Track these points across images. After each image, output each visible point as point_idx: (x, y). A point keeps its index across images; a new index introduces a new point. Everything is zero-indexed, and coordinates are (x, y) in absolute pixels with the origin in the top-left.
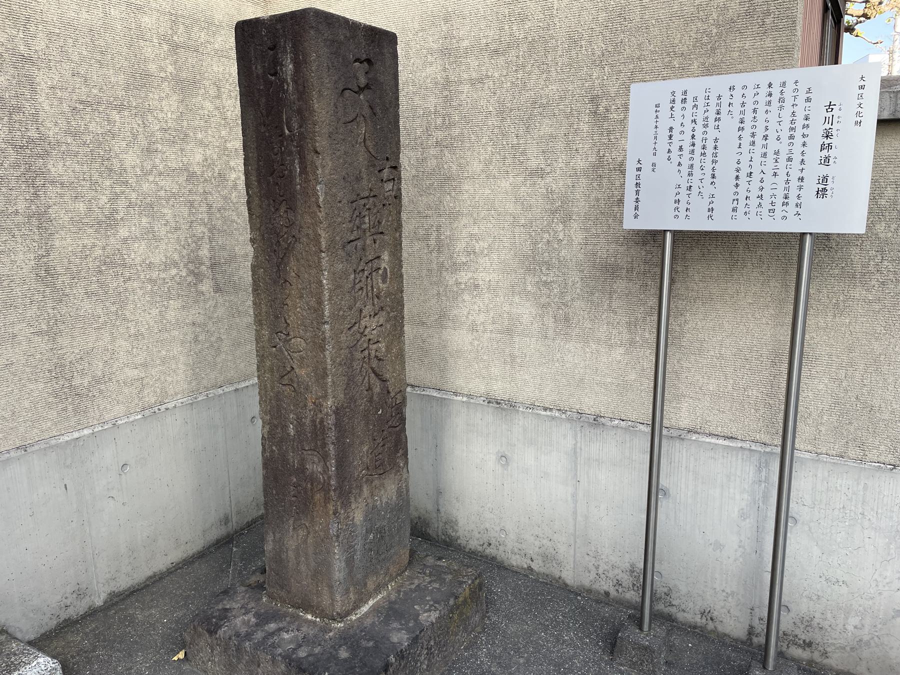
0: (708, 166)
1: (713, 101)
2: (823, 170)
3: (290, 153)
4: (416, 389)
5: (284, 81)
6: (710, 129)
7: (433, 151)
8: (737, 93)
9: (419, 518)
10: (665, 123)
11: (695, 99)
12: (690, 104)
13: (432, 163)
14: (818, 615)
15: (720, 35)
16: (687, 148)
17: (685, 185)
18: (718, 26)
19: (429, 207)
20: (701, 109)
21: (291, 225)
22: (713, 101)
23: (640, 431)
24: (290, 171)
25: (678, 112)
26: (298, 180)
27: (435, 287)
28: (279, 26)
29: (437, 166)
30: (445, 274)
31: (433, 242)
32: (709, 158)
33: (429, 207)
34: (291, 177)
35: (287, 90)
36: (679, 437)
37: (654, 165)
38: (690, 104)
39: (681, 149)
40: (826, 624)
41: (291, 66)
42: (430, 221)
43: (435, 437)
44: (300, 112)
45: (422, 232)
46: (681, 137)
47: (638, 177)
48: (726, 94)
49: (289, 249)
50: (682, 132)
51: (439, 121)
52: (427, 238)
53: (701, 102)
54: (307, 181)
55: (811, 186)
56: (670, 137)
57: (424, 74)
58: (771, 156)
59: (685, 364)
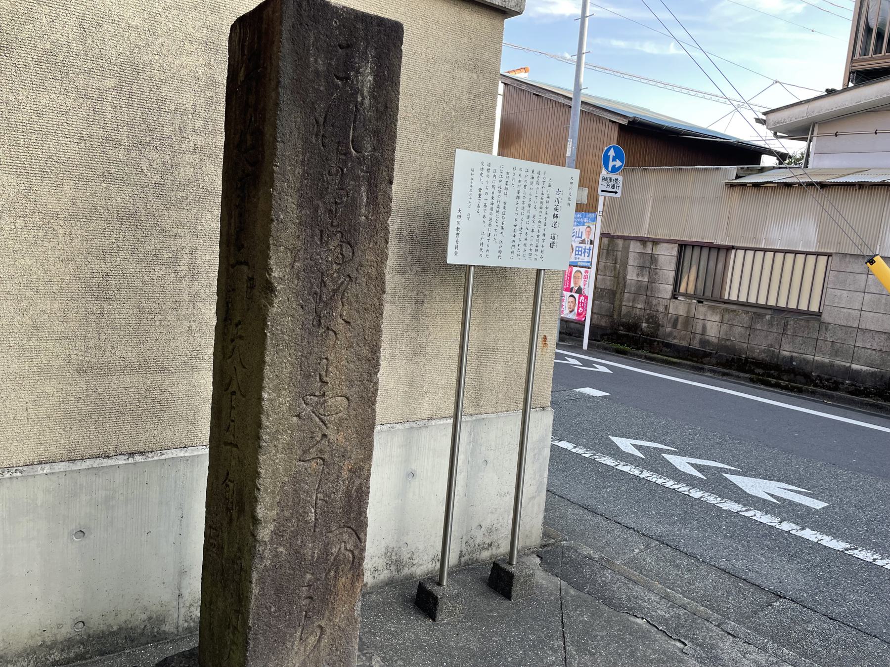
0: (500, 220)
1: (504, 175)
2: (553, 231)
3: (357, 178)
4: (150, 455)
5: (357, 91)
6: (502, 194)
7: (187, 158)
8: (517, 172)
9: (150, 618)
10: (477, 184)
11: (495, 170)
12: (491, 174)
13: (186, 172)
14: (495, 522)
15: (456, 117)
16: (489, 206)
17: (486, 233)
18: (456, 111)
19: (181, 225)
20: (498, 179)
21: (344, 261)
22: (504, 175)
23: (399, 430)
24: (354, 199)
25: (484, 179)
26: (363, 211)
27: (185, 322)
28: (360, 26)
29: (195, 175)
30: (199, 305)
31: (183, 268)
32: (501, 215)
33: (181, 225)
34: (353, 206)
35: (362, 103)
36: (425, 426)
37: (469, 215)
38: (491, 174)
39: (485, 205)
40: (498, 526)
41: (370, 78)
42: (179, 242)
43: (181, 507)
44: (376, 133)
45: (166, 255)
46: (486, 197)
47: (459, 223)
48: (511, 172)
49: (338, 292)
50: (487, 193)
51: (199, 124)
52: (174, 261)
53: (498, 174)
54: (376, 212)
55: (548, 240)
56: (480, 195)
57: (177, 62)
58: (531, 218)
59: (428, 368)
